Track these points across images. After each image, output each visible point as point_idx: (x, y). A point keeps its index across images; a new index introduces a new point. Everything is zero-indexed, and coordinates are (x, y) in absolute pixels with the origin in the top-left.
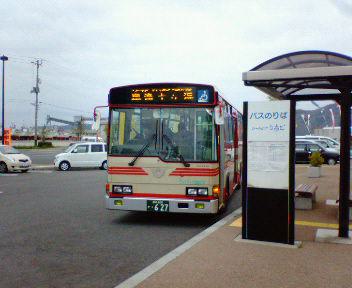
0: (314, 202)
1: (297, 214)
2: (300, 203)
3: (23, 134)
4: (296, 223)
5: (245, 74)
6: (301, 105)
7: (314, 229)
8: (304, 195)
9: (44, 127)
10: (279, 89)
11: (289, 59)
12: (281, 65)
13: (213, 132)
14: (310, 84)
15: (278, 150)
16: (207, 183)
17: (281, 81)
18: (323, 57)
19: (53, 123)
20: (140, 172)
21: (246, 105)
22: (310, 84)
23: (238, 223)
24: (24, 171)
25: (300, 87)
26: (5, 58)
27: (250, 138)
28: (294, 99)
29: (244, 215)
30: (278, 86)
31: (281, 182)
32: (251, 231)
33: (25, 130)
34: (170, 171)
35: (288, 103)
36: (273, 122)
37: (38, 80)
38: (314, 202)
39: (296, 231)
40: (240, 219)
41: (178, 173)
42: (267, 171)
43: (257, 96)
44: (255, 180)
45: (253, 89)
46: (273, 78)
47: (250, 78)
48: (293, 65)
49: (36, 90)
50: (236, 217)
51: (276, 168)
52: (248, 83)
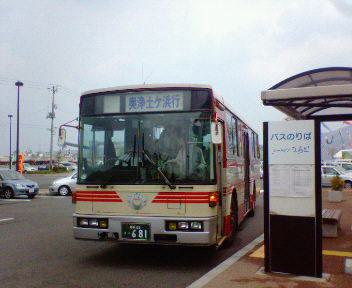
0: (339, 229)
1: (324, 243)
2: (327, 231)
3: (39, 159)
4: (325, 252)
5: (263, 93)
6: (328, 128)
7: (343, 259)
8: (331, 222)
9: (60, 153)
10: (299, 109)
11: (310, 76)
12: (303, 82)
13: (212, 151)
14: (323, 100)
15: (302, 174)
16: (201, 212)
17: (308, 100)
18: (306, 79)
19: (68, 148)
20: (115, 199)
21: (266, 125)
22: (323, 100)
23: (260, 253)
24: (31, 196)
25: (325, 106)
26: (19, 84)
27: (270, 162)
28: (319, 120)
29: (266, 242)
30: (298, 105)
31: (308, 210)
32: (272, 264)
33: (41, 155)
34: (153, 196)
35: (311, 123)
36: (296, 143)
37: (54, 106)
38: (339, 229)
39: (324, 262)
40: (263, 248)
41: (161, 198)
42: (291, 198)
43: (275, 115)
44: (278, 207)
45: (271, 108)
46: (313, 95)
47: (269, 97)
48: (314, 83)
49: (52, 116)
50: (257, 247)
51: (301, 193)
52: (267, 102)
